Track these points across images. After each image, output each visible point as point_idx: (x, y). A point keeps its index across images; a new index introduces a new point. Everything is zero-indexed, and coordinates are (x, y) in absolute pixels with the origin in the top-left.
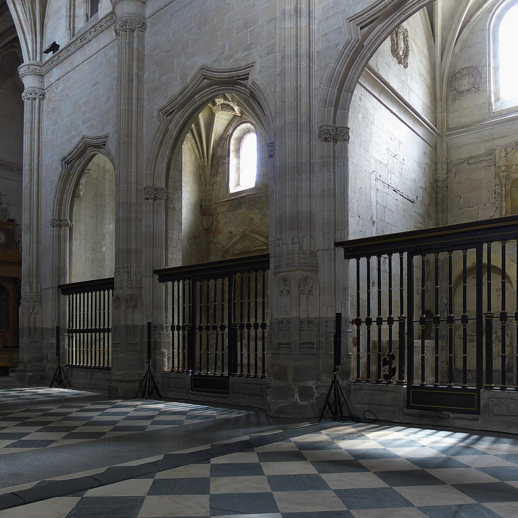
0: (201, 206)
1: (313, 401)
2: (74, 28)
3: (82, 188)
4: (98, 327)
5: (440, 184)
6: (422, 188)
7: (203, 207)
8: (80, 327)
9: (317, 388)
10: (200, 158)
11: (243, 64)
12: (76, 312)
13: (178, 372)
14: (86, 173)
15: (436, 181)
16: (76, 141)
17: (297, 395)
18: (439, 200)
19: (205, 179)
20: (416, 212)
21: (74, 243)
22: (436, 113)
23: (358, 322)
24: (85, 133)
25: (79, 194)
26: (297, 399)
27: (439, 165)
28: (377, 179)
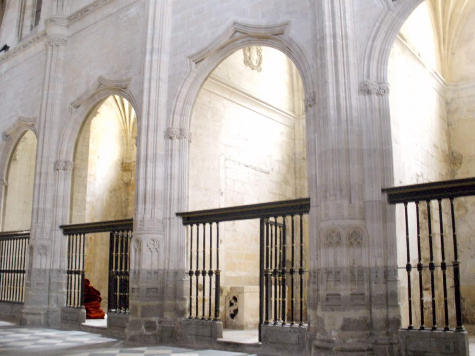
0: (122, 164)
1: (156, 332)
2: (21, 34)
3: (19, 153)
4: (8, 269)
5: (297, 156)
6: (278, 161)
7: (124, 164)
8: (9, 268)
9: (160, 322)
10: (123, 123)
11: (124, 78)
12: (7, 255)
13: (74, 307)
14: (23, 141)
15: (294, 154)
16: (14, 120)
17: (143, 327)
18: (297, 169)
19: (127, 141)
20: (270, 181)
21: (9, 197)
22: (293, 100)
23: (191, 273)
24: (21, 114)
25: (15, 157)
26: (143, 330)
27: (297, 141)
28: (226, 159)
